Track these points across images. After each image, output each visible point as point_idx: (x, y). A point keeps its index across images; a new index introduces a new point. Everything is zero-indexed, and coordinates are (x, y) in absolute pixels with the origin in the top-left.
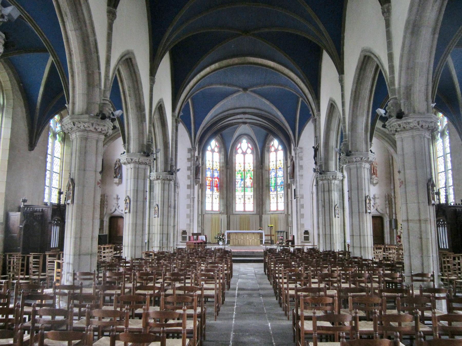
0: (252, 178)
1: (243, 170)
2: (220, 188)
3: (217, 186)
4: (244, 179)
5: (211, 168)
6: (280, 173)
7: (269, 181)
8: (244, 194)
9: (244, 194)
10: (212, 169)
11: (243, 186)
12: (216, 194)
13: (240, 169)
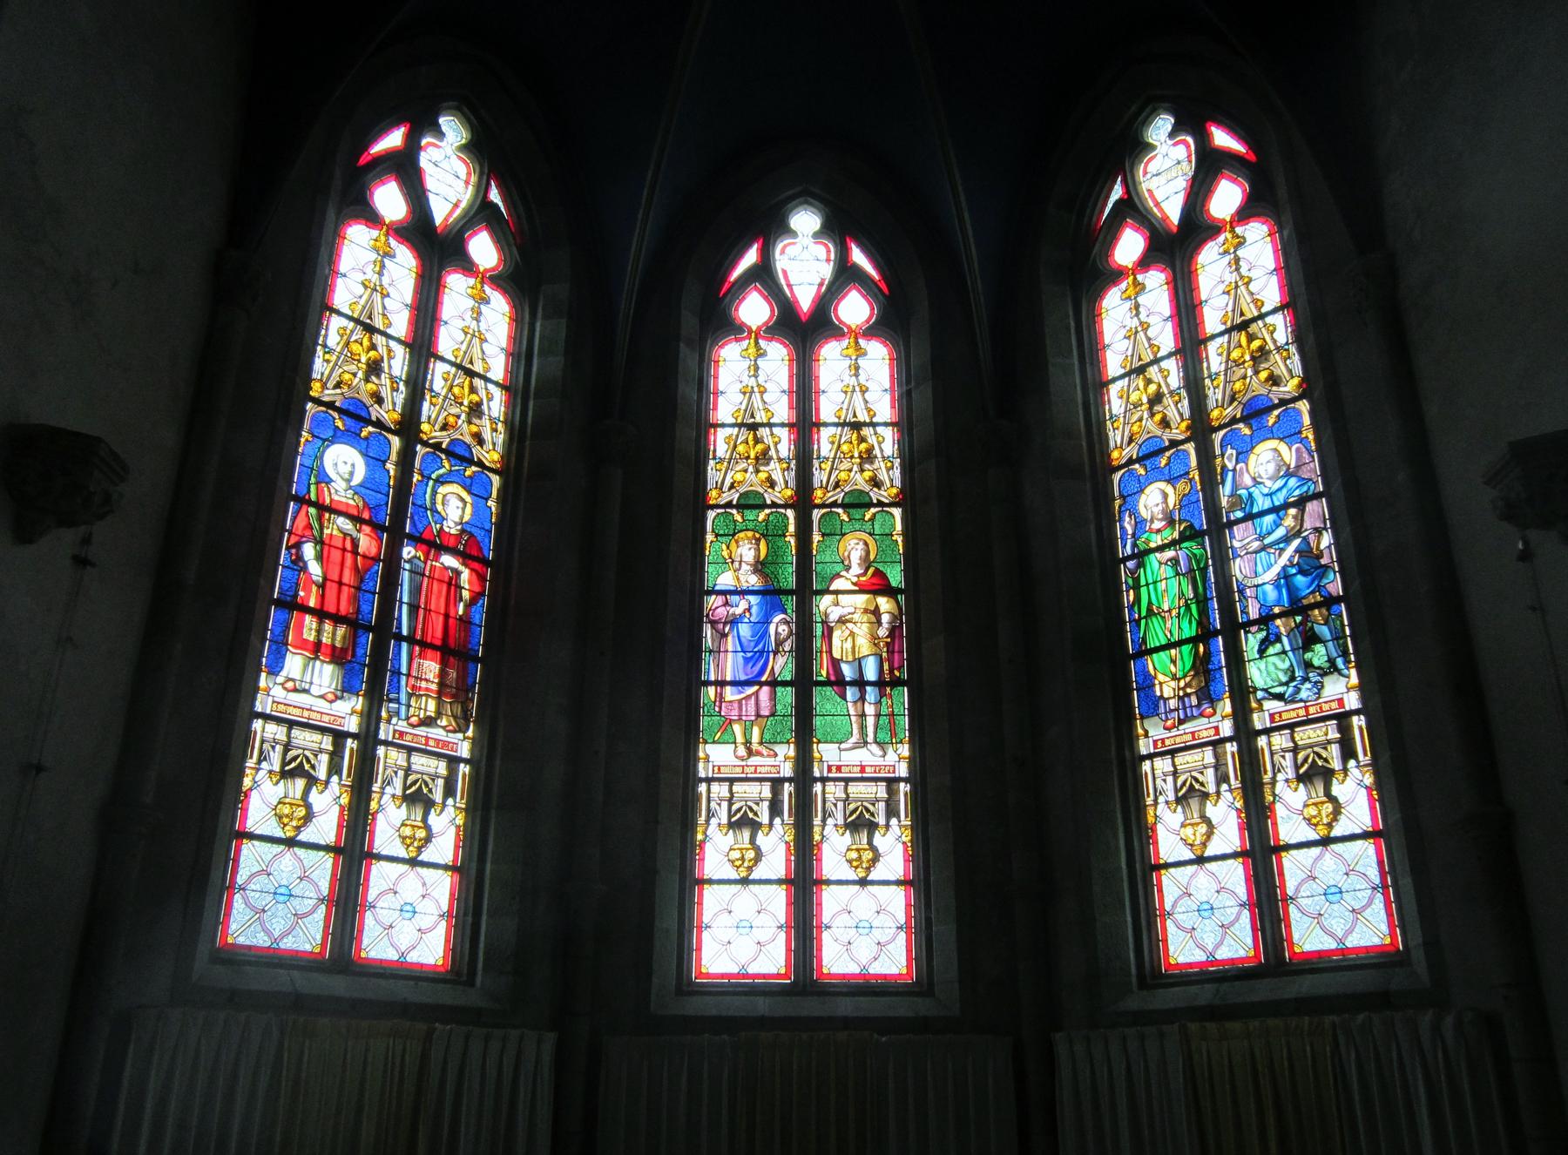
0: (896, 577)
1: (783, 492)
2: (500, 672)
3: (448, 652)
4: (806, 591)
5: (389, 413)
6: (1268, 466)
7: (1286, 261)
8: (804, 760)
9: (804, 760)
10: (408, 426)
11: (783, 666)
12: (431, 736)
13: (752, 480)
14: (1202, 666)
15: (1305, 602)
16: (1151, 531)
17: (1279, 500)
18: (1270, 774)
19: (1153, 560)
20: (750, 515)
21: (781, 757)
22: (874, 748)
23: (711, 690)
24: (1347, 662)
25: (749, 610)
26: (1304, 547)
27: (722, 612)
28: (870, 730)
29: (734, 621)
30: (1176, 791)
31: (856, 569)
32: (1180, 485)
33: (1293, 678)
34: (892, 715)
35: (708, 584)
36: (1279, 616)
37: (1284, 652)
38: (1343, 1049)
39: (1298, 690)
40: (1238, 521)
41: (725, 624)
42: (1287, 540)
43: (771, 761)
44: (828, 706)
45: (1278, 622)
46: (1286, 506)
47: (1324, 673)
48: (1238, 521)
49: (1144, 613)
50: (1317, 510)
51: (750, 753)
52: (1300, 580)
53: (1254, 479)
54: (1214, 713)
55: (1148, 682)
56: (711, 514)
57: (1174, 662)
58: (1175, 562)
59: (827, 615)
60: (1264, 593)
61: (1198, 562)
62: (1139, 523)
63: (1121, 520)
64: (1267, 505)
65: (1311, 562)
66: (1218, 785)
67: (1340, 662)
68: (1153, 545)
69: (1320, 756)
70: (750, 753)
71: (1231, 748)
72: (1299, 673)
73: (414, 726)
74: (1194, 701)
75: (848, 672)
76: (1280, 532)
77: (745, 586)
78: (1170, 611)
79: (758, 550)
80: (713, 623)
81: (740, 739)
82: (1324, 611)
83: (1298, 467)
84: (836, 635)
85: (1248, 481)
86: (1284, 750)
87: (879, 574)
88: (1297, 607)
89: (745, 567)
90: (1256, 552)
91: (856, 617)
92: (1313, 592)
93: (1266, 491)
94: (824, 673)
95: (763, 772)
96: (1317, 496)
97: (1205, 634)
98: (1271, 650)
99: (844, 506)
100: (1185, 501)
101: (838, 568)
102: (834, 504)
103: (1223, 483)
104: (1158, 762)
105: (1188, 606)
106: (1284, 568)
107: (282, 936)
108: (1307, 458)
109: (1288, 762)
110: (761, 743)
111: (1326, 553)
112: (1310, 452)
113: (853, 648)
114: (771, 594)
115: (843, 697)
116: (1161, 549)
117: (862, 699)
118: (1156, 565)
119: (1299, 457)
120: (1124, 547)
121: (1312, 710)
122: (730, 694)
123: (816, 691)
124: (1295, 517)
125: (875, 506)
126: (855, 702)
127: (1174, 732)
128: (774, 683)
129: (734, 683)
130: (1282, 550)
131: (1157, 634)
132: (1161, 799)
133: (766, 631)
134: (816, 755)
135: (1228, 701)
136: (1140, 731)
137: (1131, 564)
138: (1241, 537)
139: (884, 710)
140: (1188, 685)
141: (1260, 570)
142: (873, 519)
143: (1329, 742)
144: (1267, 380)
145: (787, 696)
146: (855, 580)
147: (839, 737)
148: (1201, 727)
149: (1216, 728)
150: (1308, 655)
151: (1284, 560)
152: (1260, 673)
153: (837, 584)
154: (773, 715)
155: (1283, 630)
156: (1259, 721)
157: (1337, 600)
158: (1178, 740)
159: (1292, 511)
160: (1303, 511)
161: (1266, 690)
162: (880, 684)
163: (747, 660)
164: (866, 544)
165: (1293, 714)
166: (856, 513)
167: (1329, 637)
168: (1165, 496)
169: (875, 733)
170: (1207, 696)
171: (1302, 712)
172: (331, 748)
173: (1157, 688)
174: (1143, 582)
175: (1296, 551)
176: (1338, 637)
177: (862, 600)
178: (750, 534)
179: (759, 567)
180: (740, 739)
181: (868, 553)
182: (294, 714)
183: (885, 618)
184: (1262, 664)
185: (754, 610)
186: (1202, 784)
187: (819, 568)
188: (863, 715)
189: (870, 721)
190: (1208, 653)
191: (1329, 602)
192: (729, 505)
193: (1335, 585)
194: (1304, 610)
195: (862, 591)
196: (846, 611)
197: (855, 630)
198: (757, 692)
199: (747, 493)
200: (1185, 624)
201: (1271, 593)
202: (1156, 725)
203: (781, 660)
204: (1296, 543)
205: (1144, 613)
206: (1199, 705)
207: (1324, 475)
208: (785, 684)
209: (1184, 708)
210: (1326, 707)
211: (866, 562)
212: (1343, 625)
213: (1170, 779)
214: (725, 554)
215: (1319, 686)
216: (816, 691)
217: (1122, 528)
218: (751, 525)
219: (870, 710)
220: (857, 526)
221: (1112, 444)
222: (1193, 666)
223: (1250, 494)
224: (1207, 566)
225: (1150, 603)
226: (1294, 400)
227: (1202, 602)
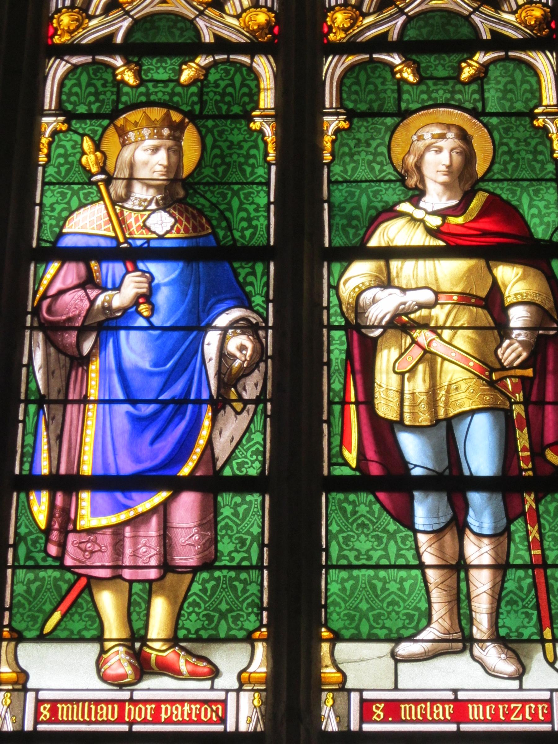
11: (234, 438)
20: (159, 70)
21: (227, 680)
22: (492, 655)
23: (40, 505)
25: (148, 297)
27: (75, 303)
28: (482, 606)
29: (108, 325)
31: (437, 198)
34: (541, 566)
35: (41, 233)
38: (239, 325)
41: (82, 332)
43: (198, 689)
44: (363, 544)
51: (143, 667)
56: (57, 69)
59: (359, 310)
70: (143, 667)
75: (415, 451)
77: (139, 236)
79: (176, 151)
80: (52, 330)
81: (114, 628)
84: (386, 359)
87: (496, 206)
89: (140, 192)
91: (439, 314)
94: (351, 457)
99: (402, 46)
101: (390, 194)
102: (381, 43)
107: (109, 125)
110: (173, 641)
113: (432, 392)
114: (210, 261)
115: (406, 519)
117: (458, 524)
122: (89, 511)
123: (330, 504)
125: (486, 46)
126: (437, 533)
128: (212, 484)
129: (100, 483)
133: (197, 347)
134: (329, 672)
139: (520, 553)
142: (481, 76)
145: (248, 517)
146: (435, 222)
147: (394, 624)
153: (392, 233)
154: (208, 564)
162: (505, 485)
163: (139, 423)
164: (464, 136)
166: (438, 65)
169: (495, 615)
177: (451, 272)
178: (156, 113)
179: (176, 192)
180: (114, 628)
181: (468, 156)
183: (518, 317)
185: (162, 298)
187: (339, 195)
188: (458, 568)
189: (481, 583)
192: (106, 45)
195: (451, 251)
196: (412, 298)
197: (438, 347)
198: (164, 510)
199: (151, 18)
203: (232, 425)
208: (242, 485)
211: (465, 180)
214: (90, 160)
216: (330, 504)
218: (159, 94)
219: (478, 552)
220: (441, 95)
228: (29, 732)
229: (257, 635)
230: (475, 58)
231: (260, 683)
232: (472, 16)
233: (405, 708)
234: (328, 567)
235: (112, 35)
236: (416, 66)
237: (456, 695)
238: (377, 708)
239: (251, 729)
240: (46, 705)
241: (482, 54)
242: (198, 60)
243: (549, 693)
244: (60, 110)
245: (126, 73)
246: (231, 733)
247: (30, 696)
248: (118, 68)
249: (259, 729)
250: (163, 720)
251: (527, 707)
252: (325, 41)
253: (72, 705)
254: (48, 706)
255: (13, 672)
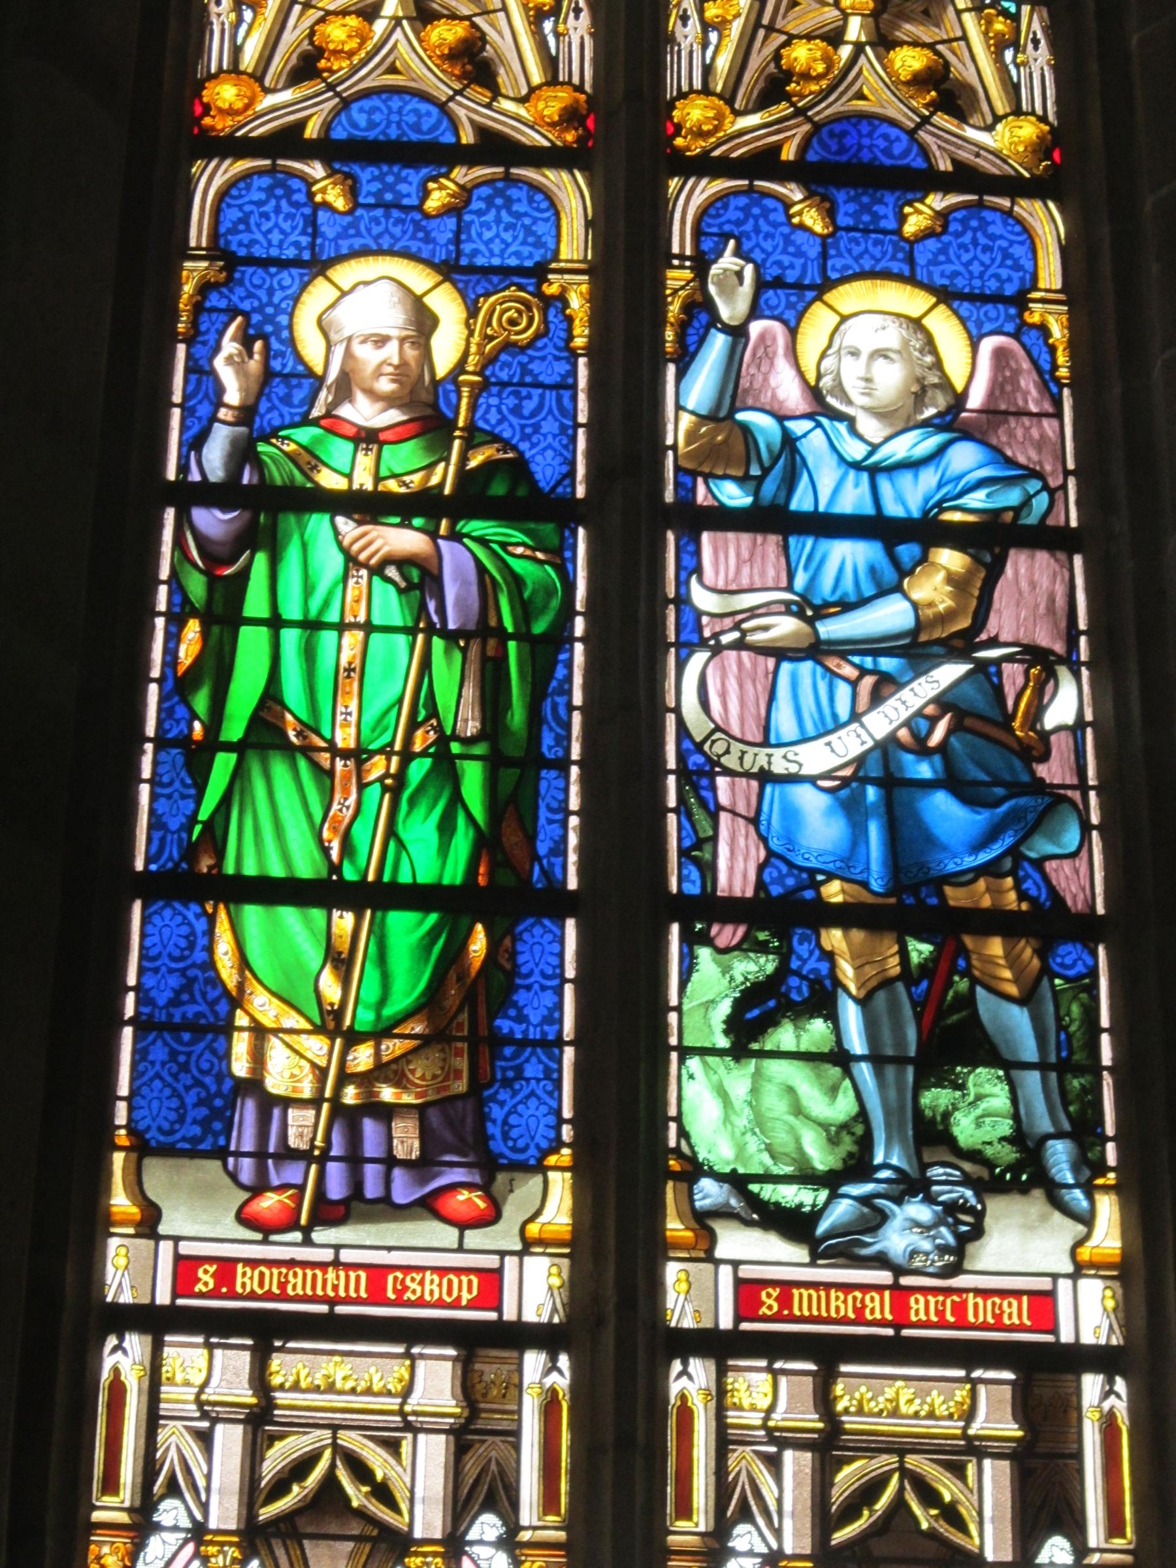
14: (467, 1015)
15: (955, 896)
16: (331, 424)
17: (906, 498)
18: (701, 1520)
19: (320, 540)
24: (1089, 1167)
26: (976, 698)
30: (253, 1493)
32: (502, 305)
33: (858, 1166)
36: (844, 916)
37: (840, 1058)
39: (873, 1219)
40: (724, 519)
42: (917, 648)
45: (834, 938)
46: (928, 531)
47: (993, 1181)
48: (724, 519)
49: (234, 730)
50: (1035, 594)
52: (945, 813)
53: (815, 393)
54: (492, 1217)
55: (199, 1015)
56: (211, 179)
57: (340, 961)
58: (420, 579)
60: (791, 814)
61: (525, 610)
62: (286, 385)
63: (203, 345)
64: (852, 499)
65: (994, 756)
66: (461, 1509)
67: (1060, 1157)
68: (329, 480)
69: (929, 1496)
71: (541, 1375)
72: (889, 1155)
73: (266, 1229)
74: (406, 1140)
76: (889, 616)
78: (359, 755)
82: (1027, 952)
83: (993, 413)
85: (788, 390)
86: (781, 1439)
88: (911, 900)
90: (780, 653)
92: (990, 870)
93: (855, 450)
95: (433, 1297)
96: (1049, 538)
97: (501, 891)
98: (784, 1037)
99: (327, 150)
100: (501, 368)
103: (685, 359)
104: (186, 1358)
105: (445, 768)
106: (887, 747)
108: (1032, 397)
109: (790, 1486)
111: (1061, 746)
112: (1047, 378)
116: (369, 506)
118: (330, 563)
119: (1003, 382)
120: (196, 443)
121: (918, 1307)
124: (957, 583)
127: (287, 1246)
130: (885, 686)
131: (280, 827)
132: (170, 1512)
135: (560, 1185)
136: (120, 1201)
137: (213, 521)
138: (724, 578)
140: (383, 1071)
141: (791, 721)
143: (975, 1448)
144: (920, 81)
148: (420, 1254)
149: (491, 1280)
150: (936, 1098)
151: (884, 721)
152: (717, 1111)
155: (847, 971)
156: (689, 1295)
157: (1086, 928)
158: (297, 1282)
159: (950, 559)
160: (994, 572)
161: (737, 1181)
165: (841, 1305)
167: (1029, 1051)
168: (423, 322)
170: (471, 1146)
171: (879, 1307)
172: (1012, 1430)
173: (241, 1045)
174: (256, 603)
175: (944, 702)
176: (1068, 1062)
182: (302, 1294)
184: (738, 1078)
186: (383, 1493)
190: (502, 977)
191: (1048, 923)
192: (764, 163)
193: (1082, 874)
194: (953, 928)
200: (420, 828)
201: (819, 827)
202: (205, 1192)
204: (949, 673)
205: (234, 730)
206: (423, 1166)
207: (1089, 471)
209: (355, 1160)
210: (979, 1310)
212: (1093, 1029)
213: (230, 1439)
215: (966, 1228)
217: (201, 371)
221: (217, 53)
222: (429, 1003)
223: (789, 442)
224: (560, 637)
225: (271, 696)
226: (1015, 187)
227: (520, 773)
228: (726, 1332)
229: (552, 1160)
230: (928, 201)
231: (561, 1244)
232: (451, 104)
233: (801, 1295)
234: (685, 1052)
235: (301, 124)
236: (349, 182)
237: (337, 1255)
238: (769, 1296)
239: (545, 1319)
240: (207, 1267)
241: (464, 170)
242: (929, 200)
243: (332, 1251)
244: (217, 250)
245: (444, 193)
246: (1067, 1345)
247: (166, 1248)
248: (317, 182)
249: (556, 1320)
250: (464, 1303)
251: (390, 1278)
252: (196, 131)
253: (817, 1291)
254: (775, 1293)
255: (687, 1229)
